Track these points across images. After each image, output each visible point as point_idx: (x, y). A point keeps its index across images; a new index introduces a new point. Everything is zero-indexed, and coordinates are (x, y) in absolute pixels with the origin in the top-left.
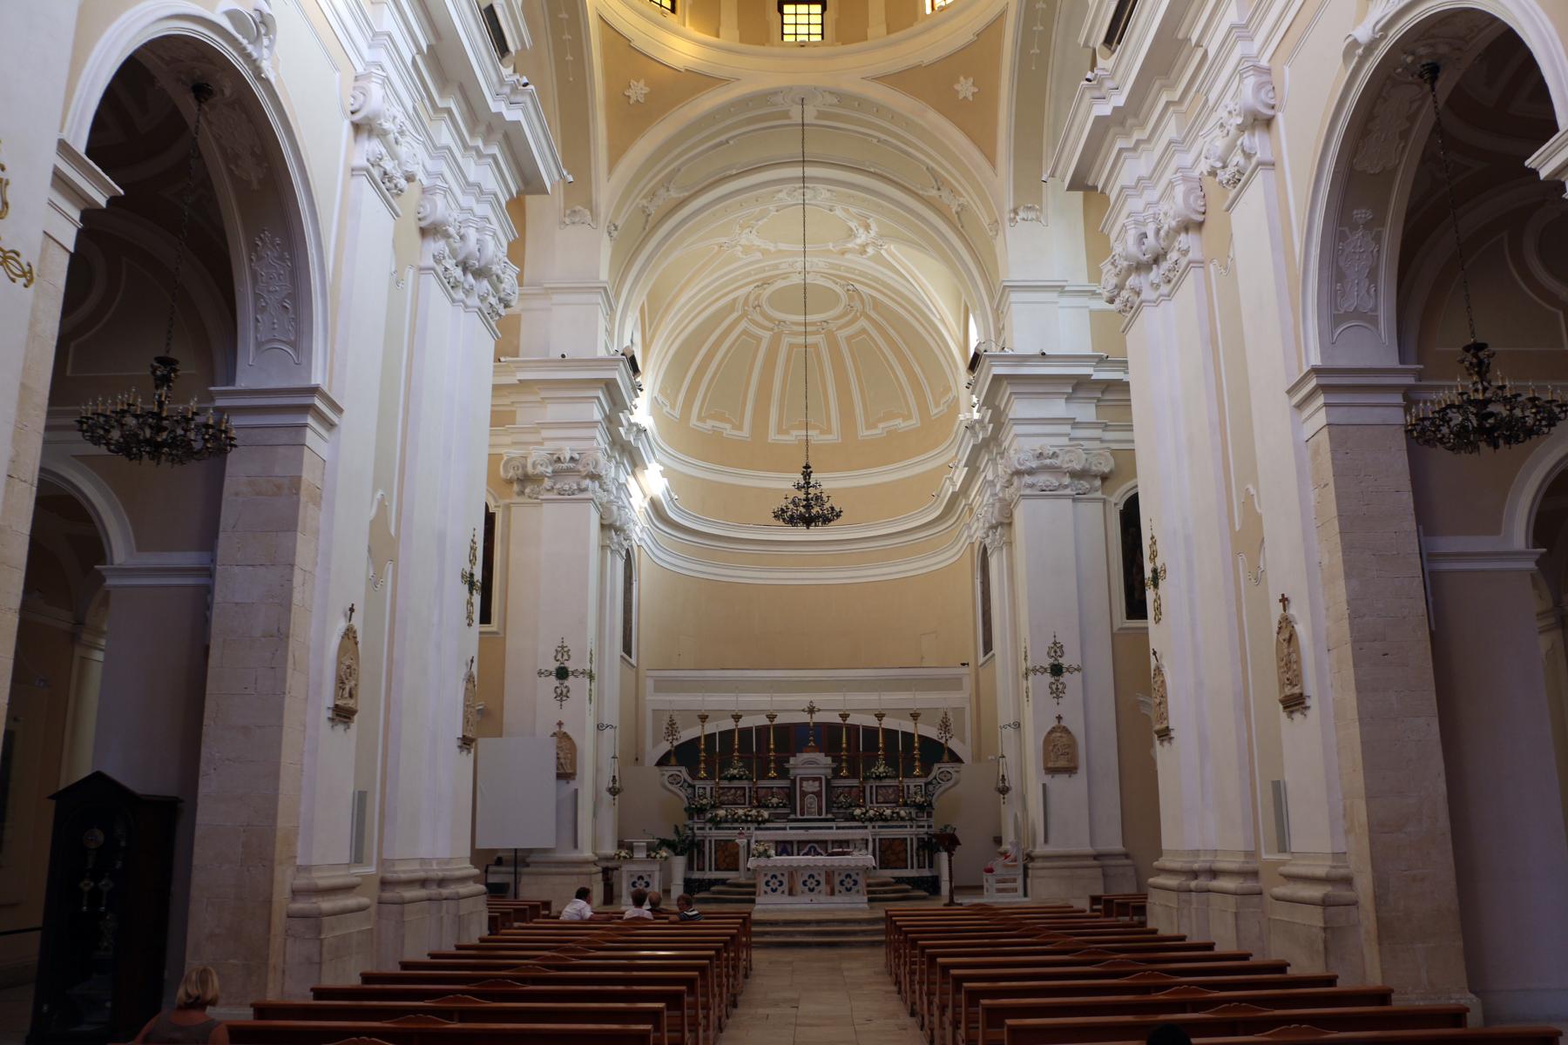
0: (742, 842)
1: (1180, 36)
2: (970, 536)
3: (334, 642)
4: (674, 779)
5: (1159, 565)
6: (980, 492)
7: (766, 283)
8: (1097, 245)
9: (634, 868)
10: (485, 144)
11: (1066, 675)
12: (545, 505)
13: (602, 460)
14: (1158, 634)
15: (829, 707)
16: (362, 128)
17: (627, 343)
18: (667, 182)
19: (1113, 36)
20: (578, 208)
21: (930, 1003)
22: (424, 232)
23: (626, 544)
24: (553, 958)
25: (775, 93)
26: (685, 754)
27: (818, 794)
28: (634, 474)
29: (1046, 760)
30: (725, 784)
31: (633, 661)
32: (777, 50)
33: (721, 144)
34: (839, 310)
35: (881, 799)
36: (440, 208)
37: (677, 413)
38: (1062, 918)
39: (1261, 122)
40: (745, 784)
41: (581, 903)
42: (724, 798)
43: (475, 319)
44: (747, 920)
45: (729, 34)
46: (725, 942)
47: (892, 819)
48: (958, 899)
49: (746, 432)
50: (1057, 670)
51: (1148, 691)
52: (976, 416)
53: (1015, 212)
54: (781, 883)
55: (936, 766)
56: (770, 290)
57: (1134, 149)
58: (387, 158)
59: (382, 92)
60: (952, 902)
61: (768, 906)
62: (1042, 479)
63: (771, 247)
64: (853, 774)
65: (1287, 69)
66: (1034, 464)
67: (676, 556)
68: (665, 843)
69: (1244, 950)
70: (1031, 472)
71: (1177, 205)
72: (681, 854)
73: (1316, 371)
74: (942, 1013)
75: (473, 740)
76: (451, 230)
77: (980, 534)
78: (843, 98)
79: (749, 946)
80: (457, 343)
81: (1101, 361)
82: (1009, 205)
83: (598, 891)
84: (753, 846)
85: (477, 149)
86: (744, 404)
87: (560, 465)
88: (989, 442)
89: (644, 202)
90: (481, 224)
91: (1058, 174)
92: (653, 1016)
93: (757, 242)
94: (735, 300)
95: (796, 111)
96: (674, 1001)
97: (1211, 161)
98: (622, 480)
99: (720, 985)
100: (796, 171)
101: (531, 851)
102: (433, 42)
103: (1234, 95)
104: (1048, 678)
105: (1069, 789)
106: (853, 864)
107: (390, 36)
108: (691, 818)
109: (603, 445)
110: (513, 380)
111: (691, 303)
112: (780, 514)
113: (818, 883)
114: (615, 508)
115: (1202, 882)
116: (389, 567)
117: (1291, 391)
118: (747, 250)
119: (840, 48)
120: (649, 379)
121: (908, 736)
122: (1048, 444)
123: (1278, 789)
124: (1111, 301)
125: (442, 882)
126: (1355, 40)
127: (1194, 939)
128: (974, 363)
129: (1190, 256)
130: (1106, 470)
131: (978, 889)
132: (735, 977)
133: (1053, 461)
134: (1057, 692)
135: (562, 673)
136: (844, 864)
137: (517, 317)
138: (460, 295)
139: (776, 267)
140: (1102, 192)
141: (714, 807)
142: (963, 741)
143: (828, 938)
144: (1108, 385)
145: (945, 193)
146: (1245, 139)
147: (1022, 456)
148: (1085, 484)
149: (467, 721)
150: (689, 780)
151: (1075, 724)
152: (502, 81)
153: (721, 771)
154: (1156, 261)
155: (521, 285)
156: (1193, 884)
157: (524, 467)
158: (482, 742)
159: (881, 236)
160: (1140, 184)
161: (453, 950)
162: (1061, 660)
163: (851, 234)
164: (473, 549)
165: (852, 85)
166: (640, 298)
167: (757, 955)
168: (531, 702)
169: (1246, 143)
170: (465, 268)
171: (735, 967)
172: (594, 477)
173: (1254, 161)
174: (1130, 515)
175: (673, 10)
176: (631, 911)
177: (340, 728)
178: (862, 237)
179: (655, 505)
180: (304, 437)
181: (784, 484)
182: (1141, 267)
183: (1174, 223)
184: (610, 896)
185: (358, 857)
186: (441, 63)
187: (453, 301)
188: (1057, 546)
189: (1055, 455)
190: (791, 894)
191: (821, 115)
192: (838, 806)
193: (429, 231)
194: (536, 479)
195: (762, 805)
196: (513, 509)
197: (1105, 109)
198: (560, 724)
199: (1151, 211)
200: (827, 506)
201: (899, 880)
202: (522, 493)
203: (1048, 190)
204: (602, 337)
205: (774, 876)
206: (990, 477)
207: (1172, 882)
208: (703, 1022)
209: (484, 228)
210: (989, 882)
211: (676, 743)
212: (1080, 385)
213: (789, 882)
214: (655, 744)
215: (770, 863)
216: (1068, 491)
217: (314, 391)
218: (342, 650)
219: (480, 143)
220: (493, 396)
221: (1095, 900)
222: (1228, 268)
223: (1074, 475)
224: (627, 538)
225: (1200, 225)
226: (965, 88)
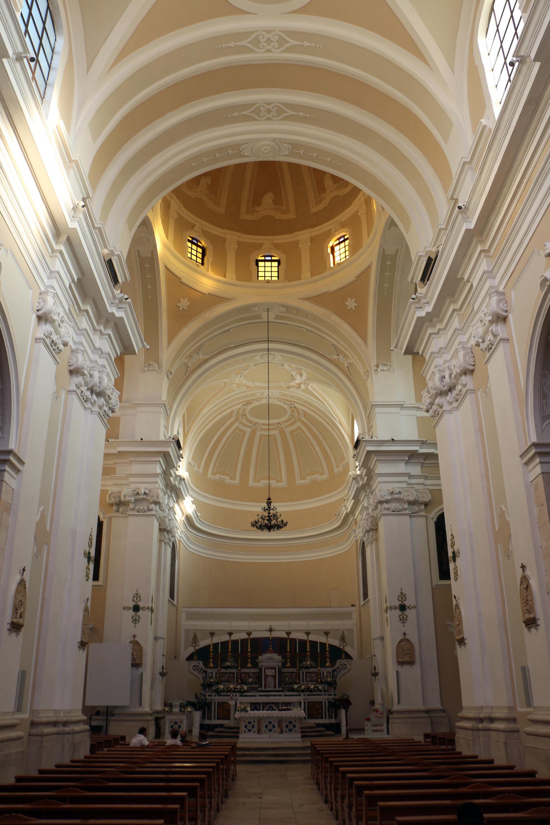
0: (232, 703)
1: (459, 277)
2: (356, 536)
3: (13, 587)
4: (196, 668)
5: (456, 549)
6: (361, 513)
7: (248, 403)
8: (420, 382)
9: (173, 717)
10: (105, 328)
11: (408, 610)
12: (130, 518)
13: (161, 494)
14: (456, 587)
15: (280, 629)
16: (43, 318)
17: (175, 433)
18: (198, 350)
19: (426, 276)
20: (151, 363)
21: (336, 795)
22: (71, 372)
23: (172, 539)
24: (126, 767)
25: (254, 306)
26: (201, 654)
27: (274, 677)
28: (177, 502)
29: (398, 656)
30: (223, 670)
31: (175, 603)
32: (255, 284)
33: (226, 331)
34: (287, 417)
35: (308, 679)
36: (80, 360)
37: (201, 471)
38: (408, 746)
39: (501, 319)
40: (234, 671)
41: (141, 737)
42: (223, 679)
43: (96, 417)
44: (234, 747)
45: (231, 276)
46: (222, 759)
47: (314, 690)
48: (351, 736)
49: (237, 481)
50: (403, 608)
51: (452, 620)
52: (358, 472)
53: (377, 366)
54: (253, 727)
55: (338, 661)
56: (251, 406)
57: (438, 333)
58: (54, 334)
59: (53, 301)
60: (347, 737)
61: (247, 739)
62: (393, 505)
63: (251, 385)
64: (293, 666)
65: (512, 292)
66: (389, 498)
67: (200, 547)
68: (190, 704)
69: (511, 763)
70: (387, 502)
71: (460, 361)
72: (199, 710)
73: (534, 445)
74: (342, 802)
75: (86, 643)
76: (86, 372)
77: (361, 535)
78: (288, 308)
79: (235, 763)
80: (86, 431)
81: (423, 443)
82: (374, 363)
83: (152, 730)
84: (238, 705)
85: (100, 331)
86: (236, 466)
87: (138, 497)
88: (365, 487)
89: (186, 360)
90: (101, 369)
91: (399, 346)
92: (180, 800)
93: (244, 382)
94: (232, 412)
95: (264, 316)
96: (192, 792)
97: (477, 339)
98: (171, 505)
99: (218, 784)
100: (265, 346)
101: (115, 707)
102: (81, 277)
103: (486, 305)
104: (398, 612)
105: (411, 673)
106: (293, 715)
107: (58, 273)
108: (204, 689)
109: (161, 486)
110: (115, 451)
111: (209, 413)
112: (254, 524)
113: (274, 726)
114: (167, 520)
115: (485, 725)
116: (45, 548)
117: (522, 456)
118: (239, 386)
119: (287, 284)
120: (186, 452)
121: (323, 645)
122: (396, 487)
123: (524, 671)
124: (428, 411)
125: (65, 724)
126: (546, 278)
127: (483, 756)
128: (357, 445)
129: (468, 387)
130: (427, 500)
131: (362, 730)
132: (227, 780)
133: (399, 496)
134: (403, 620)
135: (136, 608)
136: (288, 715)
137: (118, 419)
138: (88, 405)
139: (254, 395)
140: (422, 355)
141: (217, 683)
142: (353, 648)
143: (279, 758)
144: (427, 456)
145: (341, 357)
146: (493, 327)
147: (383, 493)
148: (416, 508)
149: (83, 632)
150: (204, 668)
151: (413, 637)
152: (114, 297)
153: (221, 663)
154: (450, 390)
155: (121, 402)
156: (480, 726)
157: (120, 497)
158: (91, 646)
159: (308, 379)
160: (441, 351)
161: (69, 763)
162: (405, 603)
163: (293, 378)
164: (91, 539)
165: (293, 302)
166: (183, 410)
167: (239, 768)
168: (119, 624)
169: (494, 329)
170: (92, 391)
171: (227, 774)
172: (157, 503)
173: (498, 338)
174: (440, 524)
175: (203, 264)
176: (169, 742)
177: (14, 635)
178: (298, 380)
179: (188, 519)
180: (3, 476)
181: (257, 509)
182: (442, 393)
183: (459, 371)
184: (159, 733)
185: (19, 708)
186: (84, 287)
187: (85, 408)
188: (402, 539)
189: (400, 493)
190: (259, 732)
191: (277, 317)
192: (285, 683)
193: (74, 372)
194: (126, 504)
195: (244, 683)
196: (113, 520)
197: (422, 313)
198: (134, 636)
199: (447, 365)
200: (280, 520)
201: (318, 725)
202: (118, 511)
203: (394, 355)
204: (162, 430)
205: (250, 723)
206: (366, 505)
207: (469, 725)
208: (208, 806)
209: (103, 371)
210: (368, 726)
211: (197, 648)
212: (412, 456)
213: (257, 726)
214: (186, 648)
215: (247, 715)
216: (407, 512)
217: (10, 452)
218: (17, 591)
219: (102, 328)
220: (104, 460)
221: (426, 736)
222: (487, 393)
223: (410, 503)
224: (173, 536)
225: (472, 371)
226: (351, 304)
